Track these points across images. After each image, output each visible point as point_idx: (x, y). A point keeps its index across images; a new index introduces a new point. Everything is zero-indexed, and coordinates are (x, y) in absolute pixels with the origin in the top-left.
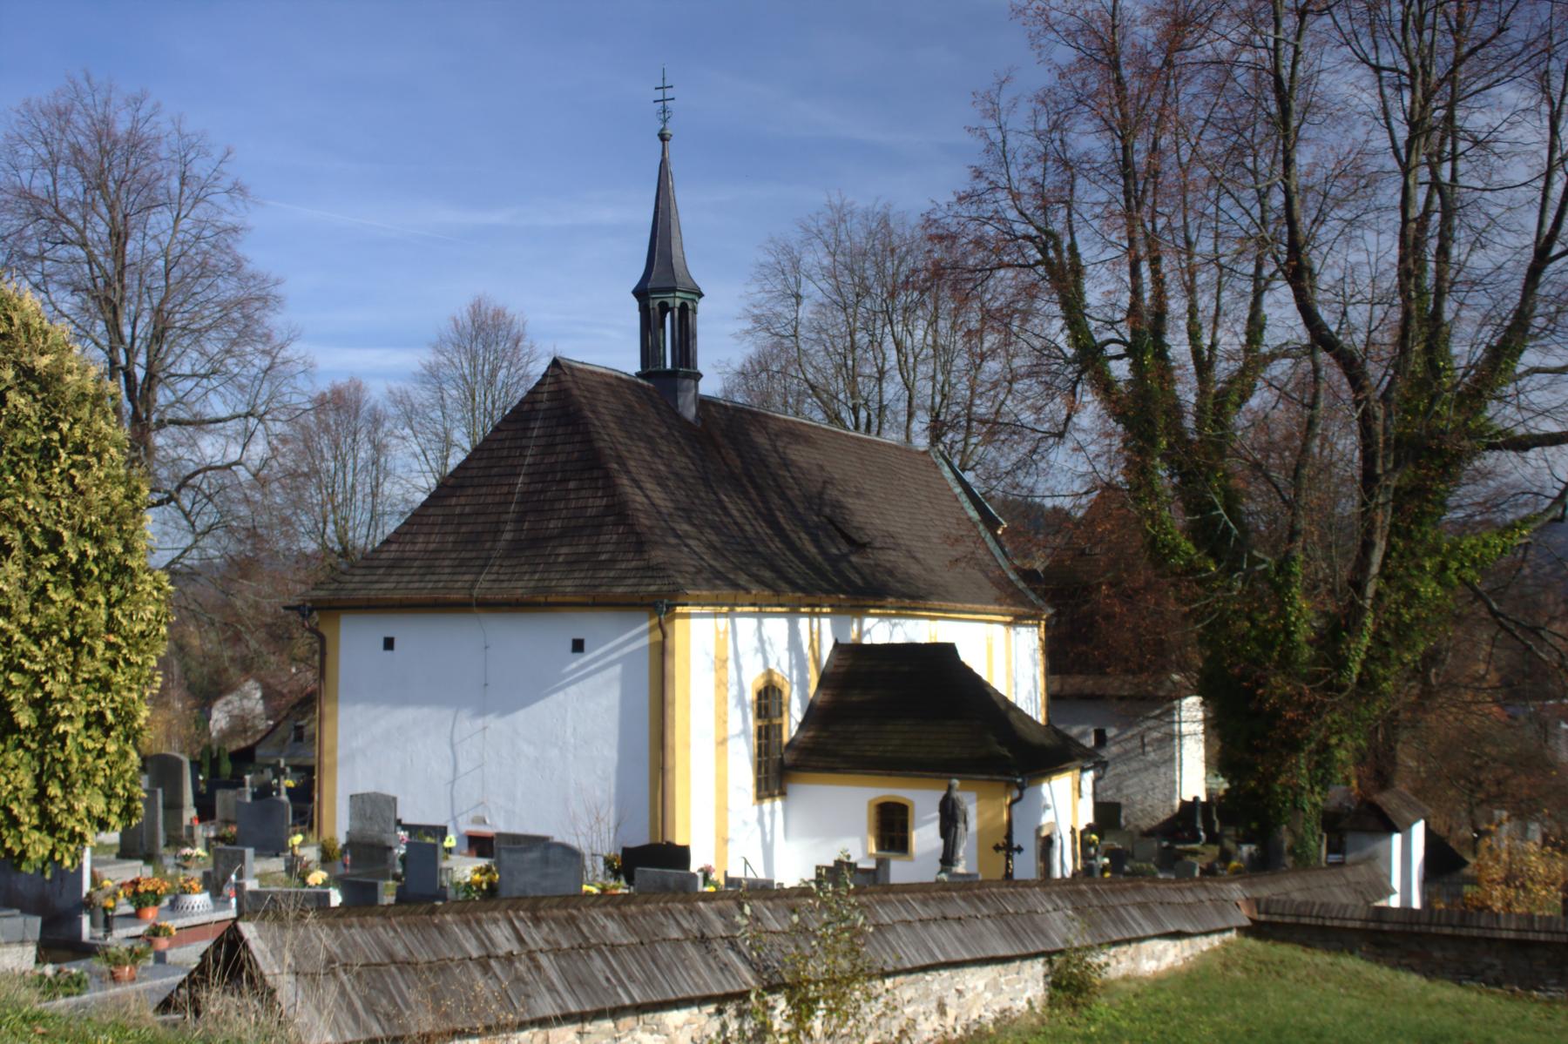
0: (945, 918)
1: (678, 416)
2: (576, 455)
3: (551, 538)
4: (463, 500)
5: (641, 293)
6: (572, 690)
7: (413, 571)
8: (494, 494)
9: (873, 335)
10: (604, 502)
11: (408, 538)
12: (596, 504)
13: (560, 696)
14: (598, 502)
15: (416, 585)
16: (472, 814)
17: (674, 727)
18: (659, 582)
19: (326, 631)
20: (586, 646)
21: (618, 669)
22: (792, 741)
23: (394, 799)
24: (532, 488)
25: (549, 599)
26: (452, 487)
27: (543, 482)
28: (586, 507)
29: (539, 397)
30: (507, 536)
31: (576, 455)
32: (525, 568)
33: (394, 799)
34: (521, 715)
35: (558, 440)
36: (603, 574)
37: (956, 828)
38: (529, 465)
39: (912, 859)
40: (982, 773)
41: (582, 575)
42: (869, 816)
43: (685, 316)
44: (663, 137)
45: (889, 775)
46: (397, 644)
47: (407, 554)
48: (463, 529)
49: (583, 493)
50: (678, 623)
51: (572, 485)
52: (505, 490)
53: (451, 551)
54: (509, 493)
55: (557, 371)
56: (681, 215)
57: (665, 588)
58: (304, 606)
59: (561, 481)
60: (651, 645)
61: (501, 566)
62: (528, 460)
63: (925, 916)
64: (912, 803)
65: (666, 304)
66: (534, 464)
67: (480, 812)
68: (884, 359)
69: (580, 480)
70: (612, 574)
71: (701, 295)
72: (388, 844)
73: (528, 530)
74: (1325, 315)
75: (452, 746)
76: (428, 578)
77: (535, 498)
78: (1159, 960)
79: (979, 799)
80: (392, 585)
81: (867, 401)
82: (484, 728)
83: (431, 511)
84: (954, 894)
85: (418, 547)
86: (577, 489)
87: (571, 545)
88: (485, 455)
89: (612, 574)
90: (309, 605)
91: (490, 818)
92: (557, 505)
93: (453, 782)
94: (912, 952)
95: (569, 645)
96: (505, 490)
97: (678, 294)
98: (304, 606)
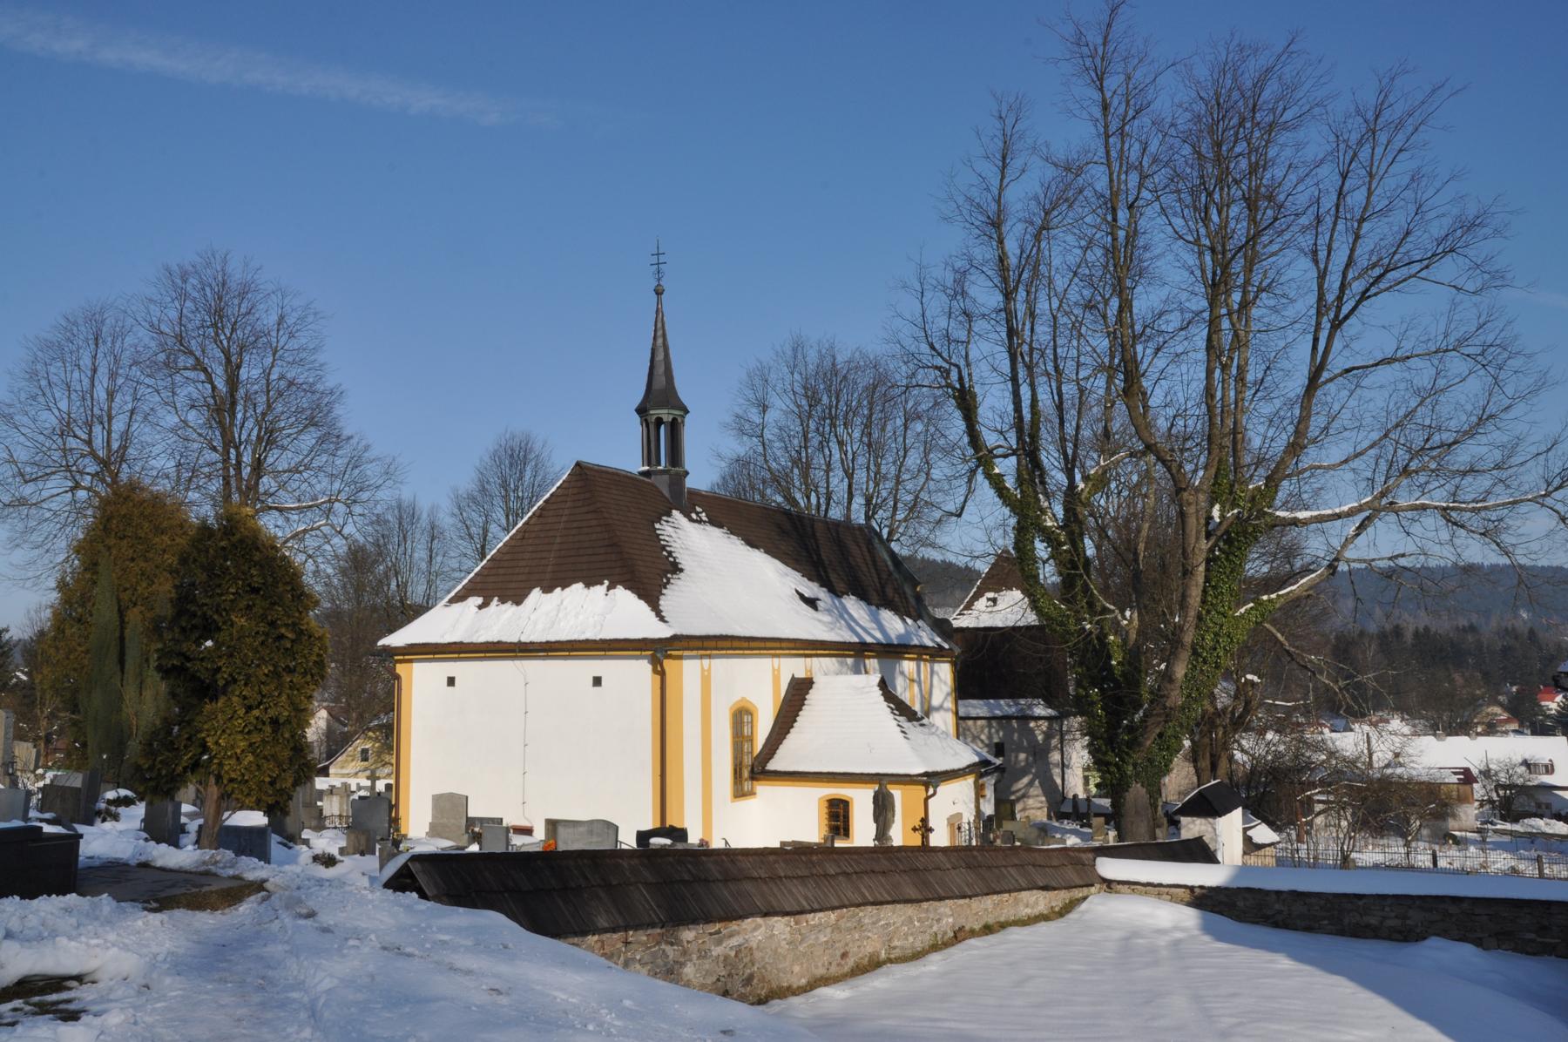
0: (873, 872)
9: (823, 435)
43: (675, 428)
44: (659, 292)
56: (724, 661)
63: (858, 870)
65: (661, 419)
68: (831, 455)
71: (687, 412)
74: (843, 622)
78: (1033, 908)
81: (817, 487)
84: (880, 856)
94: (849, 894)
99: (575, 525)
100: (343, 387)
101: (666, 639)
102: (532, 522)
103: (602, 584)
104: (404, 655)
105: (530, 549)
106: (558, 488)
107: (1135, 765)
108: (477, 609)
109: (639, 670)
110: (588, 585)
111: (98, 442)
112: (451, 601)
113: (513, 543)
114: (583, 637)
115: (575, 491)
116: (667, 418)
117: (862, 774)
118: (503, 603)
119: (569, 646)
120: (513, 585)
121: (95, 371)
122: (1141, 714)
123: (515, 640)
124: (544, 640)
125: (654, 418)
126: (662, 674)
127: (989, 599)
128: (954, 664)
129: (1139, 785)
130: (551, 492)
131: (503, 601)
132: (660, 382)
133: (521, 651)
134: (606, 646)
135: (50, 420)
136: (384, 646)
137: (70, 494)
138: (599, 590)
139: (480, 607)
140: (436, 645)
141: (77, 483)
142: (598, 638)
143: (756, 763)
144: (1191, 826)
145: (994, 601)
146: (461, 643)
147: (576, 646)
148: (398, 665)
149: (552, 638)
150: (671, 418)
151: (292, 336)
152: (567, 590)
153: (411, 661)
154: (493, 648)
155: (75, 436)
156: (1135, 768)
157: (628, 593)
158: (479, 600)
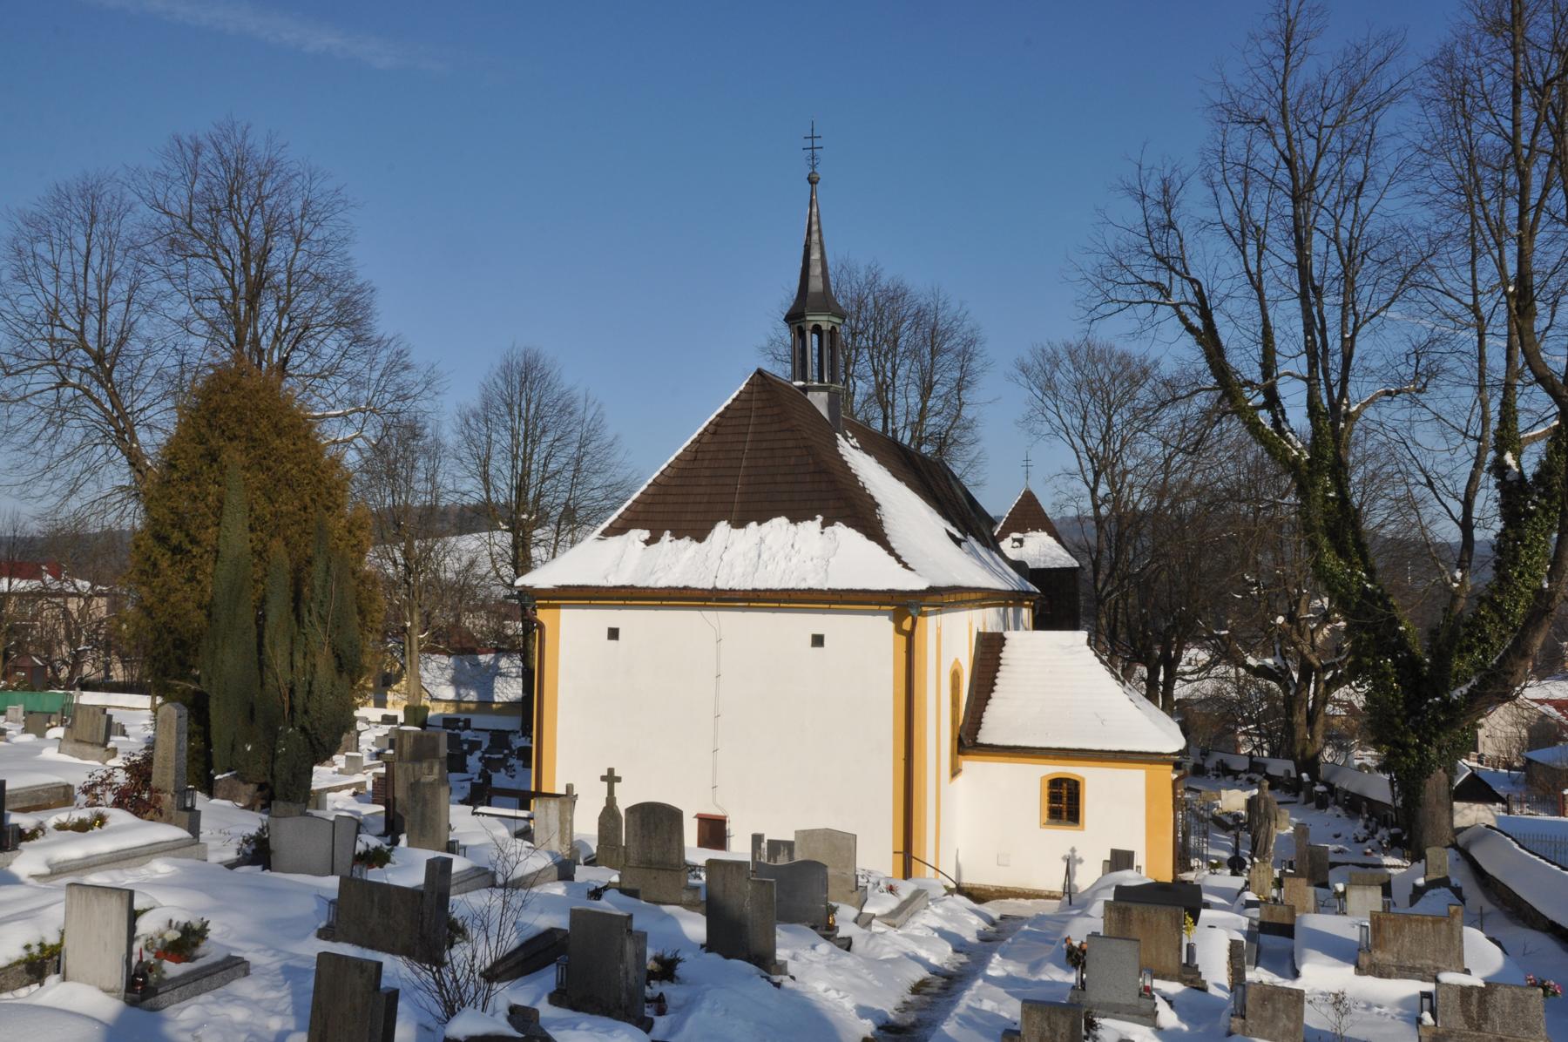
44: (812, 181)
99: (764, 445)
100: (374, 285)
101: (921, 592)
102: (705, 440)
103: (813, 519)
104: (548, 599)
105: (708, 473)
106: (734, 400)
107: (1440, 749)
108: (643, 545)
109: (879, 629)
110: (794, 520)
111: (90, 337)
112: (607, 533)
113: (682, 465)
114: (803, 586)
115: (760, 404)
116: (826, 326)
117: (1102, 751)
118: (678, 538)
119: (785, 596)
120: (689, 517)
121: (89, 252)
122: (1465, 691)
123: (709, 586)
124: (750, 588)
125: (812, 324)
126: (910, 636)
127: (1014, 540)
128: (1034, 609)
129: (1441, 771)
130: (726, 404)
131: (678, 535)
132: (816, 284)
133: (718, 600)
134: (837, 597)
135: (31, 305)
136: (523, 586)
137: (55, 391)
138: (812, 527)
139: (648, 542)
140: (598, 588)
141: (64, 378)
142: (825, 588)
143: (963, 735)
144: (1467, 811)
145: (1021, 541)
146: (632, 587)
147: (793, 596)
148: (539, 611)
149: (761, 585)
150: (830, 325)
151: (317, 224)
152: (766, 526)
153: (558, 607)
154: (678, 595)
155: (63, 326)
156: (1440, 751)
157: (852, 532)
158: (646, 534)
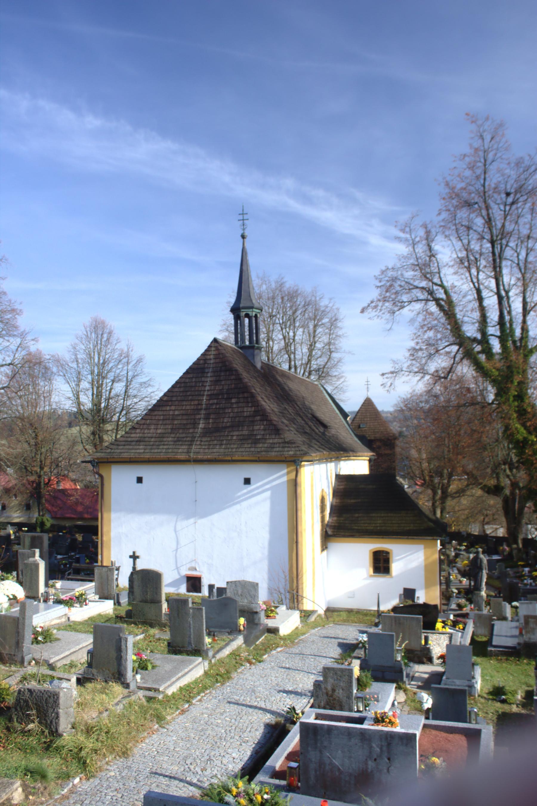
1: (254, 367)
2: (233, 386)
3: (226, 427)
4: (173, 408)
5: (235, 310)
6: (245, 504)
7: (152, 443)
8: (191, 405)
10: (253, 409)
11: (145, 426)
12: (248, 411)
13: (238, 507)
14: (249, 409)
15: (156, 451)
16: (188, 566)
17: (301, 521)
18: (293, 449)
19: (103, 472)
20: (252, 481)
21: (268, 494)
22: (328, 522)
23: (257, 584)
24: (211, 402)
25: (234, 458)
26: (166, 401)
27: (218, 399)
28: (244, 412)
29: (208, 357)
30: (201, 426)
31: (233, 386)
32: (215, 442)
33: (257, 584)
34: (215, 517)
35: (222, 378)
36: (261, 445)
37: (482, 572)
38: (208, 390)
39: (392, 577)
40: (429, 536)
41: (249, 446)
42: (370, 559)
44: (243, 237)
45: (383, 538)
46: (144, 480)
47: (146, 435)
48: (176, 422)
49: (240, 405)
50: (302, 469)
51: (234, 401)
52: (196, 402)
53: (171, 433)
54: (199, 404)
55: (216, 345)
57: (298, 453)
58: (94, 461)
59: (226, 399)
60: (288, 481)
61: (201, 441)
62: (207, 388)
64: (391, 550)
66: (210, 390)
67: (193, 565)
69: (238, 398)
70: (266, 445)
72: (255, 610)
73: (212, 423)
75: (175, 531)
76: (161, 447)
77: (214, 407)
79: (425, 548)
80: (142, 451)
82: (195, 523)
83: (156, 413)
85: (151, 431)
86: (237, 403)
87: (238, 431)
88: (183, 385)
89: (266, 445)
90: (96, 460)
91: (199, 567)
92: (227, 411)
93: (177, 550)
95: (242, 481)
96: (196, 402)
97: (254, 310)
98: (94, 461)
